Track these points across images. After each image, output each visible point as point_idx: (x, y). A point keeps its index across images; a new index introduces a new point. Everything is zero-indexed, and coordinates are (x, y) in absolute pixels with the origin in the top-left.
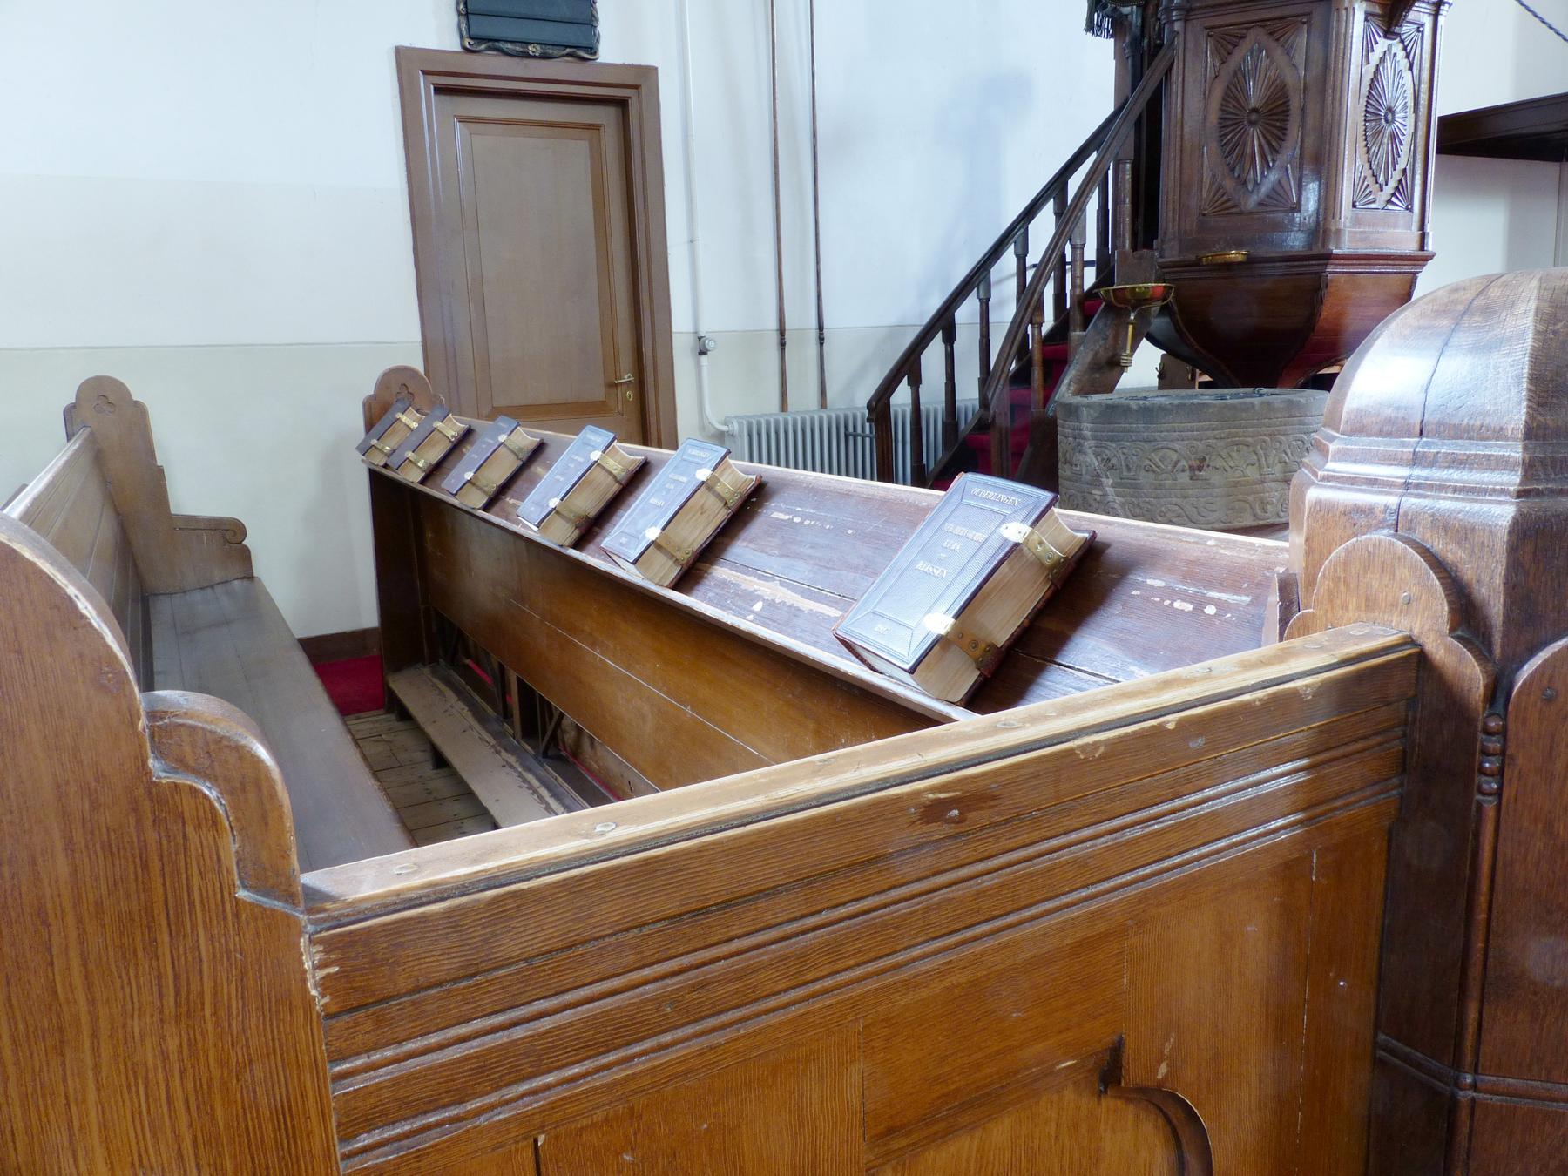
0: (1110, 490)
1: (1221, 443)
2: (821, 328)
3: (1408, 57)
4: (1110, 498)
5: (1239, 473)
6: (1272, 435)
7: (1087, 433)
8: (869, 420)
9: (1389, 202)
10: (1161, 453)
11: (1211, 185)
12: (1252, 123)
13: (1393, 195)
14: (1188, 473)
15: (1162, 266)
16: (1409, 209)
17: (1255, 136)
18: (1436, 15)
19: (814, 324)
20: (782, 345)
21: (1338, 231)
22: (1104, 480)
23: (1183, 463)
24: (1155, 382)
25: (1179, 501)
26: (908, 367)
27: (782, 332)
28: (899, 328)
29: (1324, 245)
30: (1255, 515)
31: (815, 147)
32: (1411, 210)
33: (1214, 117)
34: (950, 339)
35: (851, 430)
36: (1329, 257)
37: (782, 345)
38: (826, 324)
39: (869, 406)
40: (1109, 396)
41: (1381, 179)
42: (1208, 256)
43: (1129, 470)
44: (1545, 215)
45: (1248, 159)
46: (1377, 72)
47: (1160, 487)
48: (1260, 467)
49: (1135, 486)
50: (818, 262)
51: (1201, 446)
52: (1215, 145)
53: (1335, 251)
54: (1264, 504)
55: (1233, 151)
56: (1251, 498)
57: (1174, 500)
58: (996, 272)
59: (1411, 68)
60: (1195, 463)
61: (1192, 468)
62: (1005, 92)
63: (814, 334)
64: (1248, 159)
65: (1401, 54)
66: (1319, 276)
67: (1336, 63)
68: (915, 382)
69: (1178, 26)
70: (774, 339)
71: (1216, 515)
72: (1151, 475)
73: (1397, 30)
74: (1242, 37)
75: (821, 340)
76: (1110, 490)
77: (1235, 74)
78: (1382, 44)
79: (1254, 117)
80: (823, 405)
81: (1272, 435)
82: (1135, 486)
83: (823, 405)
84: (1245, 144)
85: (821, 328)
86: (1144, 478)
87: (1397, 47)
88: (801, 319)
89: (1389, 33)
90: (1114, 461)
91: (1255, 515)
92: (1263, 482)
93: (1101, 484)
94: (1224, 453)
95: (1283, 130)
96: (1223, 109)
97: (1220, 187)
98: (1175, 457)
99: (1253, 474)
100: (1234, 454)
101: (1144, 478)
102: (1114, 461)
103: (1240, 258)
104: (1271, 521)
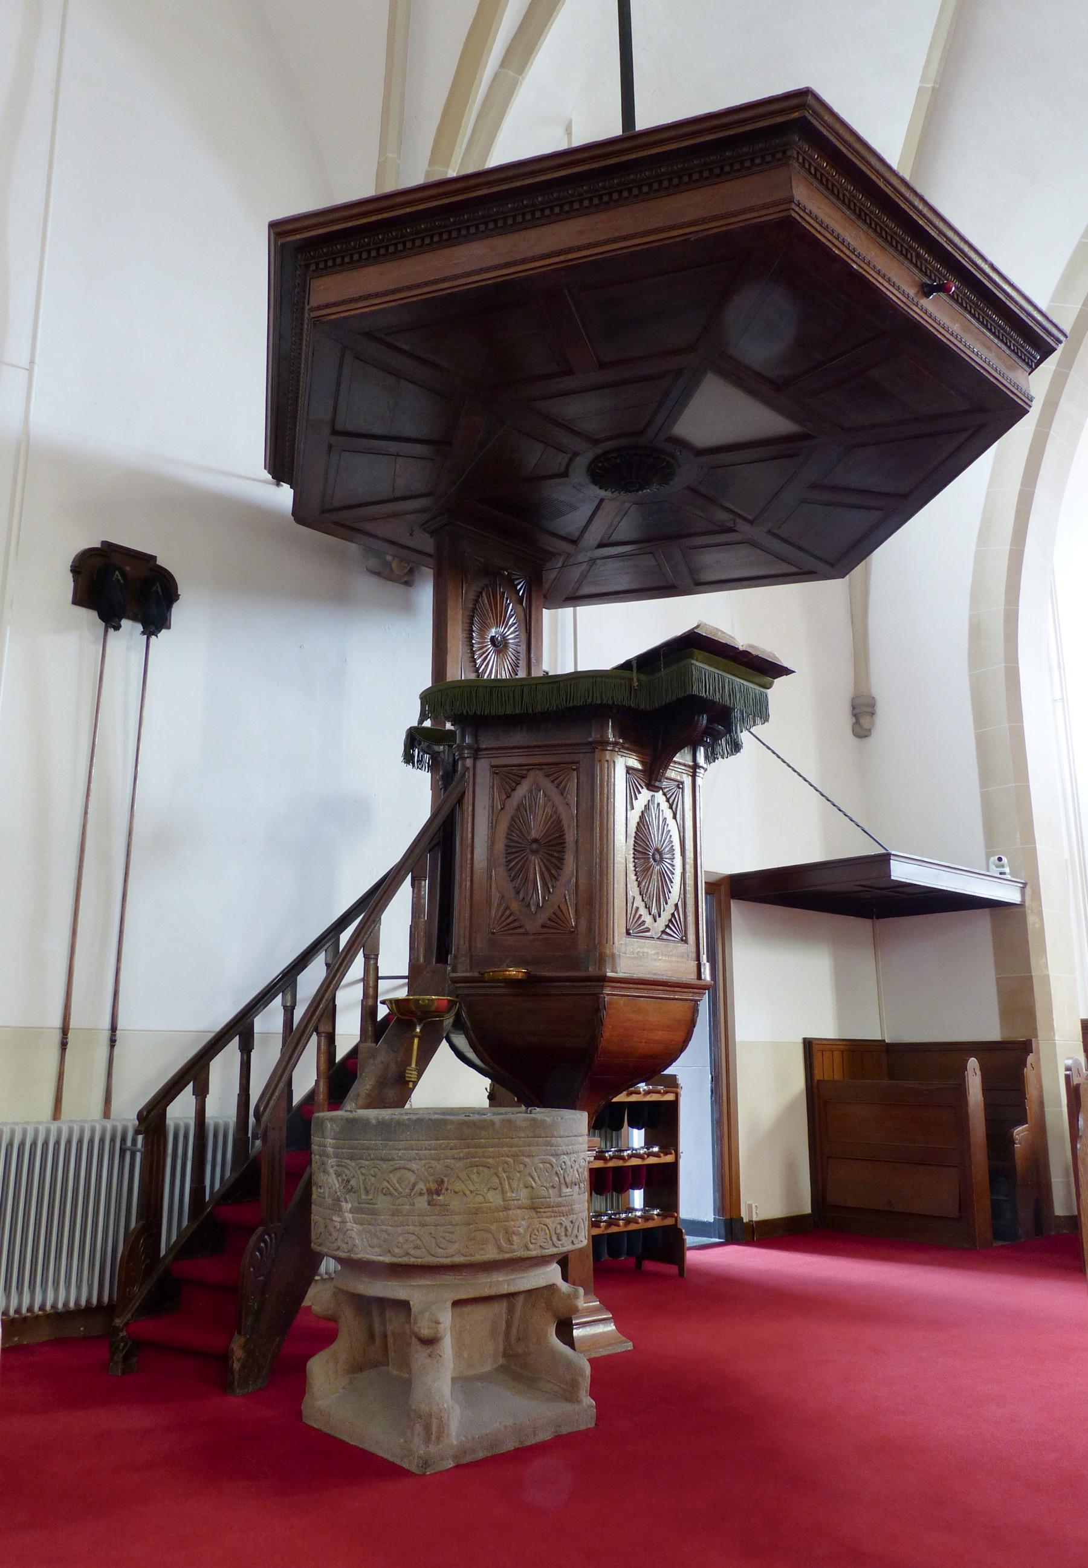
0: (349, 1216)
1: (461, 1164)
2: (114, 1029)
3: (671, 807)
4: (349, 1225)
5: (480, 1199)
6: (514, 1156)
7: (330, 1150)
8: (137, 1132)
9: (664, 932)
10: (399, 1174)
11: (500, 904)
12: (534, 852)
13: (667, 926)
14: (425, 1198)
15: (455, 981)
16: (684, 940)
17: (536, 865)
18: (694, 777)
19: (106, 1024)
20: (64, 1045)
21: (613, 955)
22: (343, 1204)
23: (421, 1186)
24: (486, 1103)
25: (417, 1229)
26: (194, 1073)
27: (65, 1031)
28: (790, 1109)
29: (600, 968)
30: (500, 1249)
31: (129, 845)
32: (686, 942)
33: (500, 846)
34: (246, 1048)
35: (129, 1143)
36: (603, 979)
37: (64, 1045)
38: (120, 1025)
39: (140, 1116)
40: (398, 1111)
41: (654, 911)
42: (490, 972)
43: (367, 1192)
44: (865, 964)
45: (531, 885)
46: (642, 817)
47: (396, 1213)
48: (503, 1192)
49: (373, 1212)
50: (119, 960)
51: (438, 1166)
52: (501, 870)
53: (609, 974)
54: (509, 1234)
55: (517, 871)
56: (493, 1227)
57: (411, 1228)
58: (302, 978)
59: (675, 817)
60: (434, 1186)
61: (430, 1192)
62: (348, 813)
63: (106, 1035)
64: (531, 885)
65: (664, 806)
66: (597, 998)
67: (602, 806)
68: (201, 1092)
69: (469, 762)
70: (57, 1036)
71: (456, 1246)
72: (389, 1199)
73: (657, 784)
74: (524, 777)
75: (113, 1042)
76: (349, 1216)
77: (518, 808)
78: (645, 795)
79: (535, 846)
80: (106, 1114)
81: (514, 1156)
82: (373, 1212)
83: (106, 1114)
84: (528, 870)
85: (114, 1029)
86: (382, 1203)
87: (659, 797)
88: (90, 1016)
89: (652, 787)
90: (353, 1182)
91: (500, 1249)
92: (506, 1209)
93: (341, 1210)
94: (463, 1175)
95: (561, 860)
96: (508, 838)
97: (507, 908)
98: (413, 1179)
99: (495, 1199)
100: (474, 1177)
101: (382, 1203)
102: (353, 1182)
103: (520, 976)
104: (518, 1254)
